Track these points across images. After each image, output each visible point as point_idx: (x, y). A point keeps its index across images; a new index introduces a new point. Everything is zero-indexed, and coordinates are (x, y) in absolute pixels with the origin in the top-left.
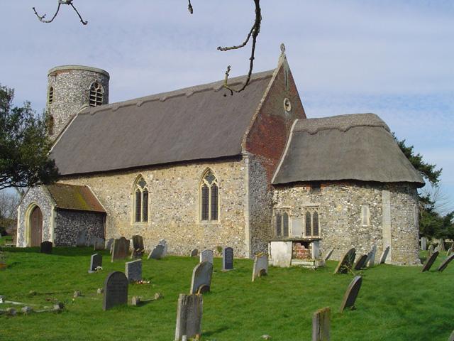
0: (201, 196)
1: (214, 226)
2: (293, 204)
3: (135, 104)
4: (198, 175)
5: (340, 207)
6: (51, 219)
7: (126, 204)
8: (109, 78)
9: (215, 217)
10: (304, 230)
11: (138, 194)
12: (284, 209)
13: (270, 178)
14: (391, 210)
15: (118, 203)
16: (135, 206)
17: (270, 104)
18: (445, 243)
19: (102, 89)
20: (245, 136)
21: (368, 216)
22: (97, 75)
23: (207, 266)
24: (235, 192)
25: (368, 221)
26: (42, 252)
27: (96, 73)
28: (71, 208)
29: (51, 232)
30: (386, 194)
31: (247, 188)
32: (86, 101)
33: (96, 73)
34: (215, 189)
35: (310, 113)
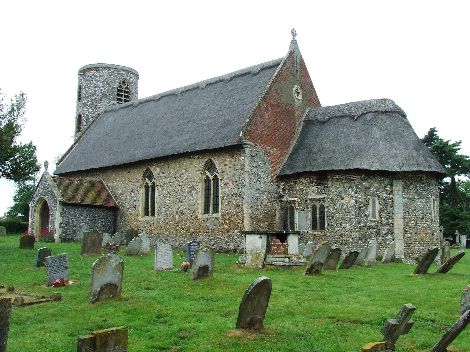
1: (215, 219)
2: (299, 196)
4: (200, 167)
7: (135, 198)
9: (216, 211)
10: (310, 223)
11: (147, 187)
14: (404, 202)
15: (129, 197)
21: (378, 207)
22: (124, 73)
27: (124, 70)
28: (79, 202)
29: (57, 226)
32: (113, 99)
33: (124, 70)
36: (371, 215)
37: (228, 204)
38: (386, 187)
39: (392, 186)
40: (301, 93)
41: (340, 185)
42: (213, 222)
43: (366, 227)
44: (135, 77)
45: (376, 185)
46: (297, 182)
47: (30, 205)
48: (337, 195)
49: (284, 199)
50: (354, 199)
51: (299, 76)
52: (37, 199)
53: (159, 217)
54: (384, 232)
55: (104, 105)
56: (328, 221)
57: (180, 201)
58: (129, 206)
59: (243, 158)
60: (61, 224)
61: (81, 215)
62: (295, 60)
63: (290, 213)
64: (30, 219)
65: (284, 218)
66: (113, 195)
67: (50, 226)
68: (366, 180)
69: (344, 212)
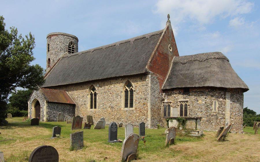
0: (124, 95)
3: (90, 52)
5: (200, 101)
7: (85, 100)
8: (78, 40)
9: (131, 106)
10: (179, 113)
11: (91, 94)
13: (161, 85)
16: (90, 101)
17: (162, 46)
19: (75, 46)
20: (149, 62)
21: (217, 106)
22: (72, 38)
23: (134, 138)
24: (143, 93)
27: (71, 37)
29: (45, 113)
31: (150, 91)
33: (71, 37)
34: (132, 91)
35: (181, 54)
36: (213, 110)
37: (139, 103)
38: (222, 96)
39: (225, 95)
40: (172, 48)
41: (196, 95)
42: (131, 113)
43: (210, 115)
44: (77, 41)
45: (217, 94)
46: (172, 93)
47: (28, 103)
48: (194, 99)
49: (166, 101)
50: (204, 101)
51: (171, 40)
52: (32, 100)
53: (99, 109)
54: (220, 118)
55: (61, 55)
56: (189, 112)
57: (111, 101)
58: (81, 104)
59: (147, 80)
60: (47, 112)
61: (57, 108)
63: (168, 108)
64: (29, 110)
65: (164, 111)
66: (72, 98)
67: (41, 114)
68: (211, 92)
69: (198, 108)
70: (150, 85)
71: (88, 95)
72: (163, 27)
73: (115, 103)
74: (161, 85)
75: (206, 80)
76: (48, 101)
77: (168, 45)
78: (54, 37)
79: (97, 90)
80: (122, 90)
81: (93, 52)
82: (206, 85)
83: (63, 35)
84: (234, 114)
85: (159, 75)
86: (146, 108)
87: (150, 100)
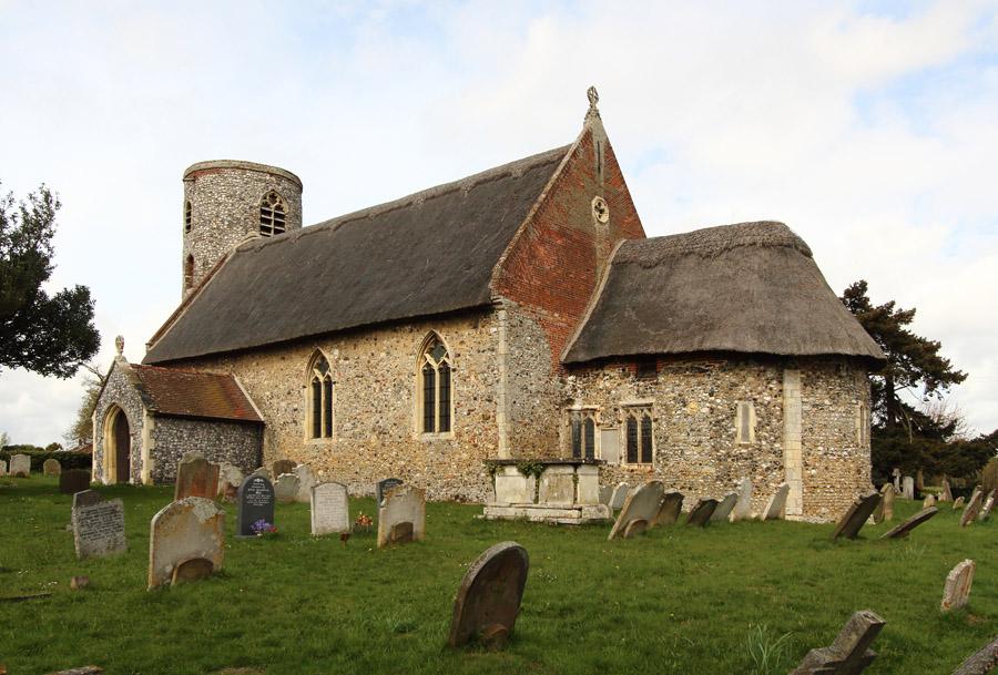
0: (422, 387)
3: (329, 229)
5: (693, 405)
6: (144, 434)
7: (296, 406)
8: (300, 187)
9: (445, 427)
10: (623, 451)
11: (317, 386)
12: (585, 411)
18: (271, 522)
19: (284, 205)
21: (753, 421)
22: (273, 179)
25: (752, 433)
26: (62, 492)
27: (272, 175)
29: (144, 456)
30: (793, 393)
31: (502, 368)
33: (272, 175)
36: (739, 436)
38: (769, 383)
39: (781, 382)
40: (607, 210)
45: (750, 379)
46: (598, 375)
48: (674, 399)
49: (577, 406)
51: (602, 179)
52: (105, 407)
54: (764, 466)
55: (235, 241)
59: (495, 329)
61: (191, 435)
62: (596, 148)
63: (586, 433)
65: (575, 442)
68: (731, 370)
70: (502, 348)
71: (304, 387)
72: (563, 133)
73: (390, 414)
74: (555, 349)
75: (709, 326)
76: (156, 412)
77: (593, 198)
78: (209, 177)
79: (333, 370)
80: (414, 369)
81: (337, 228)
82: (708, 345)
83: (242, 167)
84: (820, 453)
85: (545, 312)
86: (490, 433)
87: (502, 403)
